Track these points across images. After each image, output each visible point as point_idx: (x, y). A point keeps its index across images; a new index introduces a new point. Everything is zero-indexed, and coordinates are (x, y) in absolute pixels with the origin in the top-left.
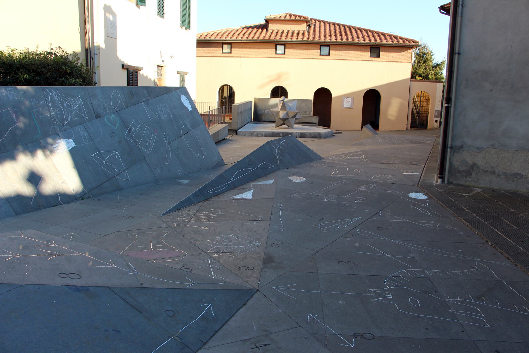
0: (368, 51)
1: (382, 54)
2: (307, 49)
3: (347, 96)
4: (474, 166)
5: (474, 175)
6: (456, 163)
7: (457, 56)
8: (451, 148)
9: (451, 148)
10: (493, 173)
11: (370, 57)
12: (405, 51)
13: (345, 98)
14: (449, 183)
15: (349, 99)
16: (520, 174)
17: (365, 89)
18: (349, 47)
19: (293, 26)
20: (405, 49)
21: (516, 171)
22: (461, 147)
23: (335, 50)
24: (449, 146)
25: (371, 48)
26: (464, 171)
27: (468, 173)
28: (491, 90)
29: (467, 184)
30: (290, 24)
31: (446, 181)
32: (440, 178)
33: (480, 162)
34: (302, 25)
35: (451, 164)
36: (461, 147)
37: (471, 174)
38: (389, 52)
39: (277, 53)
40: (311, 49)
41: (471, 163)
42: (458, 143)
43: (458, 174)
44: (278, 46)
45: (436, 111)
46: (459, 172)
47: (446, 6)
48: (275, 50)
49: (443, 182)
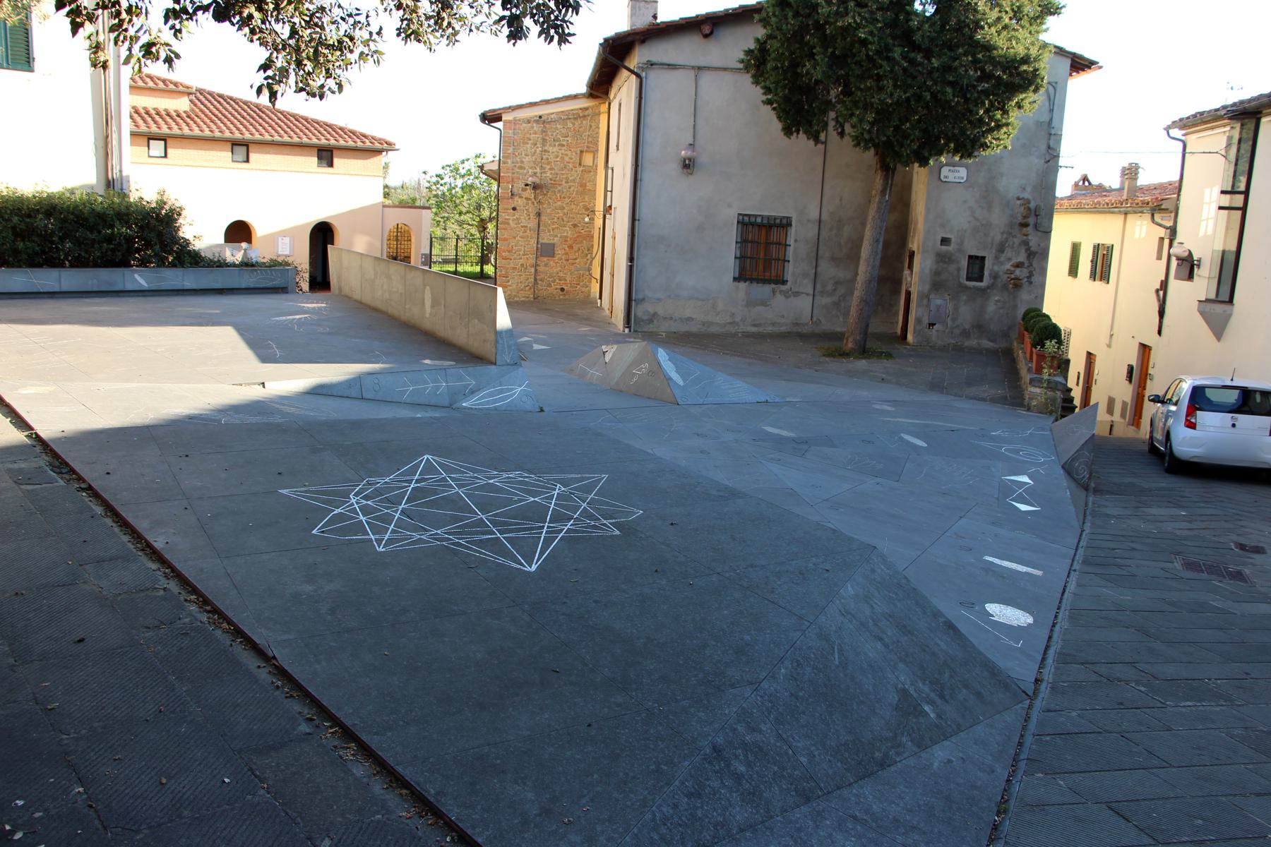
0: (314, 156)
1: (336, 161)
2: (208, 150)
3: (283, 234)
4: (655, 314)
5: (655, 321)
6: (640, 314)
7: (637, 222)
8: (635, 300)
9: (635, 300)
10: (671, 318)
11: (318, 166)
12: (373, 157)
13: (280, 239)
14: (634, 331)
15: (287, 240)
16: (691, 318)
17: (315, 221)
18: (283, 148)
19: (163, 100)
20: (373, 154)
21: (689, 316)
22: (643, 300)
23: (259, 152)
24: (634, 299)
25: (319, 150)
26: (647, 320)
27: (651, 321)
28: (666, 251)
29: (650, 330)
30: (155, 97)
31: (632, 331)
32: (627, 327)
33: (660, 311)
34: (179, 100)
35: (635, 315)
36: (643, 300)
37: (653, 321)
38: (348, 158)
39: (151, 155)
40: (216, 150)
41: (652, 312)
42: (640, 296)
43: (641, 323)
44: (151, 142)
45: (422, 255)
46: (643, 321)
47: (488, 114)
48: (147, 148)
49: (630, 331)
